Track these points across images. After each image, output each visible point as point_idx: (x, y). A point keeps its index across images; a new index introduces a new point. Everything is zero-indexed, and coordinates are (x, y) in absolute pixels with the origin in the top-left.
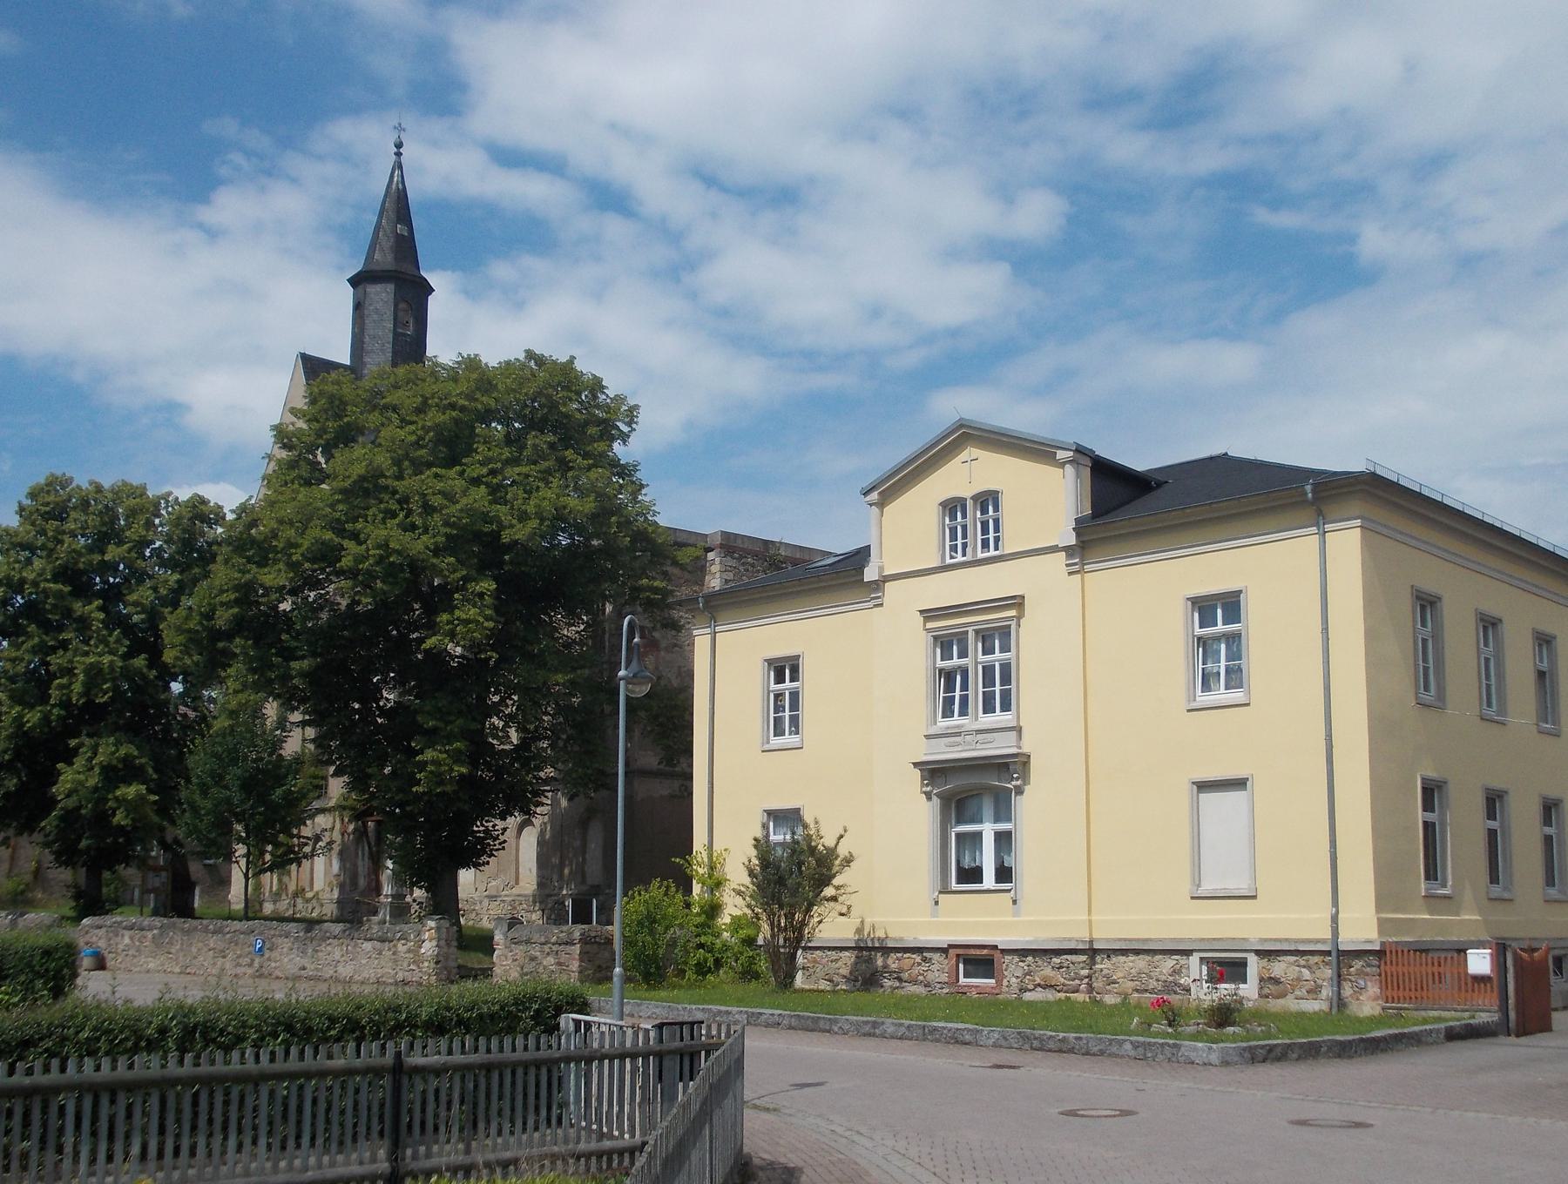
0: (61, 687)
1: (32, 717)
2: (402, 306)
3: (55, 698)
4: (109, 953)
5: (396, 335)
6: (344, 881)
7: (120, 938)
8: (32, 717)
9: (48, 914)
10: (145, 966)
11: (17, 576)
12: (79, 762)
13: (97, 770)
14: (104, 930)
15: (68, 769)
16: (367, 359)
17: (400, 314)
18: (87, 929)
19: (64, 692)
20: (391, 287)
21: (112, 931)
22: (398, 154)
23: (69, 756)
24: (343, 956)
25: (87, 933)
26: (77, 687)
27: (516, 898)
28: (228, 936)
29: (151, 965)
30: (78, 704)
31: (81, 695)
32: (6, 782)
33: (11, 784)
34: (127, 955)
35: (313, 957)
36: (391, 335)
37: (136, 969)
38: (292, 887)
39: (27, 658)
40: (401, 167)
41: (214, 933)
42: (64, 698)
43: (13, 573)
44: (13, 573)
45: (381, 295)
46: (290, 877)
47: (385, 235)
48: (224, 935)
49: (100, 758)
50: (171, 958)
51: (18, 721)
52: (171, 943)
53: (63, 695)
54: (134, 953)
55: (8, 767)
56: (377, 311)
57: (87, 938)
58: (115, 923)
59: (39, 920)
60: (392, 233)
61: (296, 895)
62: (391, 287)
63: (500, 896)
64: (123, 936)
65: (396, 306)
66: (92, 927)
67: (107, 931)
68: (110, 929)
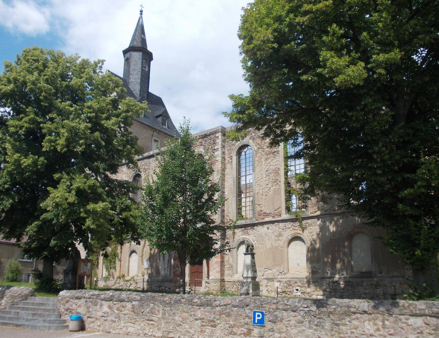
0: (50, 141)
1: (27, 161)
2: (144, 61)
3: (47, 147)
4: (88, 317)
5: (142, 70)
6: (152, 273)
7: (98, 307)
8: (27, 161)
9: (26, 288)
10: (124, 329)
11: (22, 79)
12: (62, 187)
13: (73, 192)
14: (83, 300)
15: (55, 191)
16: (130, 76)
17: (144, 63)
18: (67, 299)
19: (53, 144)
20: (141, 54)
21: (90, 301)
22: (141, 14)
23: (55, 184)
24: (378, 330)
25: (67, 302)
26: (62, 141)
27: (292, 279)
28: (218, 309)
29: (131, 329)
30: (62, 152)
31: (63, 146)
32: (4, 202)
33: (8, 203)
34: (106, 320)
35: (332, 330)
36: (141, 69)
37: (114, 332)
38: (117, 274)
39: (26, 126)
40: (142, 18)
41: (202, 305)
42: (52, 148)
43: (19, 77)
44: (19, 77)
45: (137, 56)
46: (115, 270)
47: (138, 37)
48: (213, 307)
49: (75, 186)
50: (152, 324)
51: (17, 163)
52: (152, 312)
53: (51, 146)
54: (114, 319)
55: (7, 192)
56: (135, 61)
57: (67, 306)
58: (93, 295)
59: (20, 292)
60: (140, 37)
61: (119, 278)
62: (141, 54)
63: (277, 278)
64: (101, 305)
65: (142, 60)
66: (72, 298)
67: (86, 302)
68: (88, 300)
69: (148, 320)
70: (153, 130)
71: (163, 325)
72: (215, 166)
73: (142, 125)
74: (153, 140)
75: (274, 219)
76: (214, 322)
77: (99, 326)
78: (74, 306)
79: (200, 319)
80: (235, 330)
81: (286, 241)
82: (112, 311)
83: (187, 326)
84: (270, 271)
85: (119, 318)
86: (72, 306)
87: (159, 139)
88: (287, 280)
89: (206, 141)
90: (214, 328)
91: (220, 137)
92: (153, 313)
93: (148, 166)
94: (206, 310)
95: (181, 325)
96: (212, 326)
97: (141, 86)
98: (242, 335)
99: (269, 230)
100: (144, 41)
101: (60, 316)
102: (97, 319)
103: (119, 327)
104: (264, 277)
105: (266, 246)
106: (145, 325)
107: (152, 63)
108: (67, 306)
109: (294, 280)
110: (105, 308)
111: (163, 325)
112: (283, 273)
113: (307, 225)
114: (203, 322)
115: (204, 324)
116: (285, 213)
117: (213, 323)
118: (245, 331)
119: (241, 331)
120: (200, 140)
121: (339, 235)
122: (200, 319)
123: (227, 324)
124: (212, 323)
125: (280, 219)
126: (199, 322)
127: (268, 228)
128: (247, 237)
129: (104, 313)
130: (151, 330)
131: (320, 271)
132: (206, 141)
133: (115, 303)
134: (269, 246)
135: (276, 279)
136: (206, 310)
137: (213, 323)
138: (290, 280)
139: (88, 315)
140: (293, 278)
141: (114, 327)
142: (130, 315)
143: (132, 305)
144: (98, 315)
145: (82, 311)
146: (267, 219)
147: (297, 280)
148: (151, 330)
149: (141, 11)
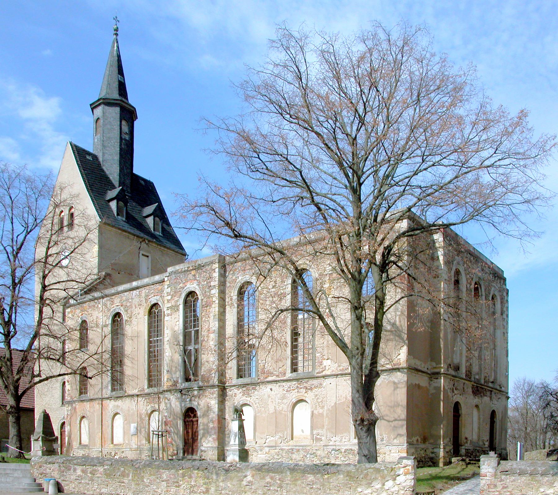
4: (64, 480)
14: (56, 465)
20: (117, 110)
57: (42, 470)
64: (75, 470)
69: (119, 482)
70: (141, 240)
71: (133, 486)
72: (211, 309)
73: (124, 233)
74: (141, 254)
75: (278, 379)
76: (178, 483)
77: (74, 488)
78: (48, 470)
79: (166, 481)
80: (195, 489)
81: (290, 404)
82: (86, 474)
83: (155, 487)
84: (272, 438)
85: (93, 480)
86: (45, 470)
87: (150, 252)
88: (289, 448)
89: (200, 274)
90: (178, 488)
91: (217, 270)
92: (124, 476)
93: (130, 302)
94: (171, 473)
95: (149, 486)
96: (176, 486)
97: (120, 167)
98: (202, 493)
99: (273, 392)
100: (122, 88)
101: (35, 481)
102: (71, 482)
103: (93, 489)
104: (266, 444)
105: (268, 410)
106: (117, 487)
107: (136, 123)
108: (42, 470)
109: (297, 448)
110: (79, 472)
111: (133, 486)
112: (286, 440)
113: (313, 386)
114: (168, 483)
115: (170, 485)
116: (290, 372)
117: (177, 484)
118: (204, 490)
119: (201, 490)
120: (193, 272)
121: (345, 399)
122: (166, 481)
123: (189, 484)
124: (176, 484)
125: (285, 378)
126: (164, 483)
127: (271, 389)
128: (248, 399)
129: (78, 476)
130: (123, 491)
131: (323, 438)
132: (200, 274)
133: (88, 467)
134: (272, 410)
135: (278, 446)
136: (171, 473)
137: (177, 484)
138: (293, 448)
139: (62, 478)
140: (296, 446)
141: (88, 488)
142: (102, 478)
143: (104, 470)
144: (72, 478)
145: (56, 475)
146: (270, 379)
147: (300, 448)
148: (123, 491)
149: (117, 30)
